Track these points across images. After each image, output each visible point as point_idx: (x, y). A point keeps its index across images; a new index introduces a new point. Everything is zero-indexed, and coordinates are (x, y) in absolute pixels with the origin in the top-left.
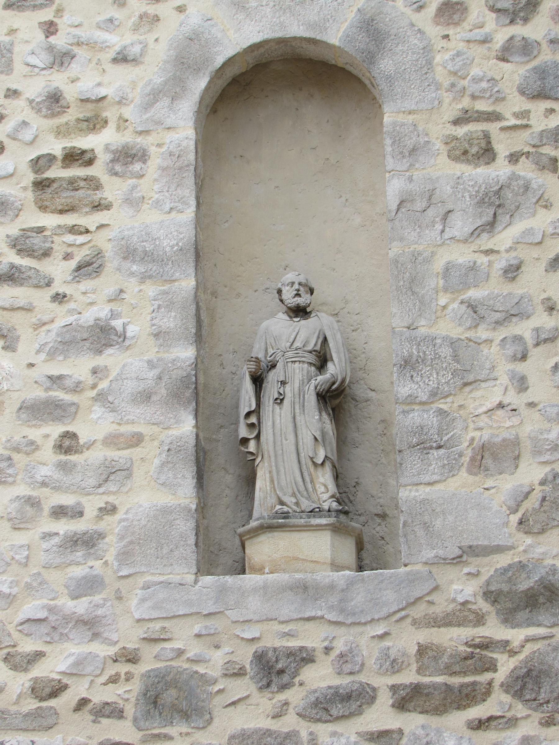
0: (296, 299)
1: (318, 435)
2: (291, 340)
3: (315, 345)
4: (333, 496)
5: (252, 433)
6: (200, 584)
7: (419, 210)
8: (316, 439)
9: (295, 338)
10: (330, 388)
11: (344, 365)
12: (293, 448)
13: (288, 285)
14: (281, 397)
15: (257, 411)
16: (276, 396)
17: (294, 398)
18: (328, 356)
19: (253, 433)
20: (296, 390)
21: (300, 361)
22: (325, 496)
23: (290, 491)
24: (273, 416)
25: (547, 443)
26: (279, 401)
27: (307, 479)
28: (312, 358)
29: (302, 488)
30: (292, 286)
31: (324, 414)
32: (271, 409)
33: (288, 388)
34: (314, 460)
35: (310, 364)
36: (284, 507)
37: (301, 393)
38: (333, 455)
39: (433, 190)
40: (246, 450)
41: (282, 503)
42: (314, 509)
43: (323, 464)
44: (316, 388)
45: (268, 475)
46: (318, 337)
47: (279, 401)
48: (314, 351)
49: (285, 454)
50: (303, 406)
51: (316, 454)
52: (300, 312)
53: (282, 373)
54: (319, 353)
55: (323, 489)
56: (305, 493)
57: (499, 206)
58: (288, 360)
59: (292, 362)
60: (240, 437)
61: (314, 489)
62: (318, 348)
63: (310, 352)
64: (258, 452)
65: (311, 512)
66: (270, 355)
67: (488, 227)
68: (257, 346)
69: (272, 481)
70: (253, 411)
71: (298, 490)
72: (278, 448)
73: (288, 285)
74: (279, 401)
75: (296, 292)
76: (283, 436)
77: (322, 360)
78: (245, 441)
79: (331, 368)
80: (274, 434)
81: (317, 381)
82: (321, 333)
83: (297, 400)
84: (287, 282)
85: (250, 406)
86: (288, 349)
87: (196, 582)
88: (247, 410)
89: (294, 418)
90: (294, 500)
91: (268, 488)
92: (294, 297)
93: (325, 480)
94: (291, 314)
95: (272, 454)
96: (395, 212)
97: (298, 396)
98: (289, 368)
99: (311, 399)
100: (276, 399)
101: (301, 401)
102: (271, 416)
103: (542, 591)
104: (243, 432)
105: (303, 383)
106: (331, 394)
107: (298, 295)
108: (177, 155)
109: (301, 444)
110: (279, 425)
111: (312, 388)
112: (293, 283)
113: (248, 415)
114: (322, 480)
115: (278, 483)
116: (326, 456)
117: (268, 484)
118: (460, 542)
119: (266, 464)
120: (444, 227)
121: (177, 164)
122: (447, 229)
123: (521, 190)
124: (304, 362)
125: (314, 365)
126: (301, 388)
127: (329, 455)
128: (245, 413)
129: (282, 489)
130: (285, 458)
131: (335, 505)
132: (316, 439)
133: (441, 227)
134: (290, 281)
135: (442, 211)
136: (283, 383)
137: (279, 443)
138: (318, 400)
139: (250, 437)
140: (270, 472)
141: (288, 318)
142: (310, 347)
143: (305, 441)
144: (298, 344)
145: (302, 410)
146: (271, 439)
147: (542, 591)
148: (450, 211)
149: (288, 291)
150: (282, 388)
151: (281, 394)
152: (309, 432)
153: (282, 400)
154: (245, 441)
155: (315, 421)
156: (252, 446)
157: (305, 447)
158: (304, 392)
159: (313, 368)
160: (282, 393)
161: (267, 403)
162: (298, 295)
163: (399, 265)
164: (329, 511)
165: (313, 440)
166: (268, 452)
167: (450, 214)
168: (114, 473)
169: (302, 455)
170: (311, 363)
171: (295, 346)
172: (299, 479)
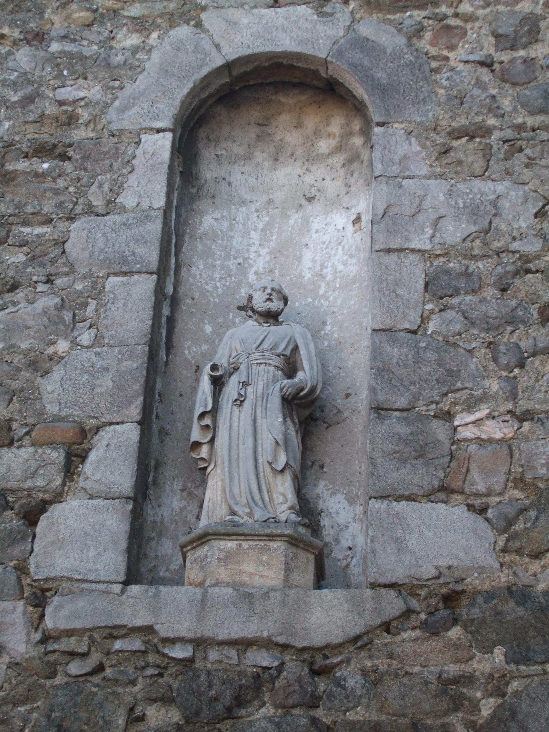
0: (267, 303)
1: (280, 438)
2: (259, 341)
3: (285, 349)
4: (292, 508)
5: (204, 438)
6: (128, 593)
7: (407, 214)
8: (277, 443)
9: (263, 341)
10: (298, 394)
11: (315, 373)
12: (250, 452)
13: (260, 290)
14: (242, 399)
15: (214, 412)
16: (236, 397)
17: (256, 401)
18: (299, 366)
19: (207, 437)
20: (260, 392)
21: (266, 364)
22: (284, 507)
23: (244, 501)
24: (231, 419)
25: (544, 457)
26: (240, 402)
27: (264, 488)
28: (278, 361)
29: (257, 497)
30: (264, 291)
31: (289, 422)
32: (229, 411)
33: (250, 389)
34: (273, 465)
35: (277, 367)
36: (236, 517)
37: (265, 396)
38: (295, 464)
39: (424, 196)
40: (198, 457)
41: (233, 513)
42: (268, 519)
43: (282, 471)
44: (281, 390)
45: (220, 484)
46: (289, 343)
47: (238, 403)
48: (283, 355)
49: (240, 460)
50: (266, 409)
51: (276, 459)
52: (271, 317)
53: (245, 373)
54: (289, 359)
55: (281, 499)
56: (260, 503)
57: (495, 215)
58: (252, 362)
59: (257, 364)
60: (192, 441)
61: (271, 499)
62: (288, 353)
63: (279, 356)
64: (211, 459)
65: (265, 521)
66: (233, 356)
67: (483, 234)
68: (220, 352)
69: (224, 491)
70: (209, 412)
71: (254, 501)
72: (234, 453)
73: (260, 290)
74: (238, 403)
75: (267, 297)
76: (241, 440)
77: (290, 367)
78: (197, 445)
79: (300, 375)
80: (230, 437)
81: (283, 385)
82: (292, 340)
83: (259, 403)
84: (259, 287)
85: (206, 406)
86: (254, 351)
87: (123, 592)
88: (201, 410)
89: (255, 421)
90: (247, 510)
91: (219, 498)
92: (266, 302)
93: (283, 490)
94: (261, 321)
95: (226, 458)
96: (381, 216)
97: (261, 399)
98: (254, 371)
99: (276, 402)
100: (236, 400)
101: (264, 404)
102: (228, 418)
103: (533, 621)
104: (196, 435)
105: (267, 386)
106: (299, 402)
107: (270, 300)
108: (151, 153)
109: (262, 474)
110: (237, 429)
111: (277, 389)
112: (265, 288)
113: (202, 415)
114: (281, 489)
115: (231, 491)
116: (287, 464)
117: (219, 493)
118: (438, 561)
119: (219, 471)
120: (434, 232)
121: (150, 162)
122: (438, 235)
123: (520, 201)
124: (270, 364)
125: (282, 370)
126: (265, 391)
127: (291, 463)
128: (199, 413)
129: (233, 497)
130: (241, 464)
131: (293, 517)
132: (277, 443)
133: (431, 232)
134: (262, 285)
135: (433, 216)
136: (246, 384)
137: (234, 447)
138: (283, 405)
139: (203, 441)
140: (222, 481)
141: (257, 324)
142: (280, 350)
143: (265, 446)
144: (265, 346)
145: (264, 414)
146: (226, 442)
147: (533, 621)
148: (441, 217)
149: (259, 296)
150: (244, 389)
151: (242, 396)
152: (270, 436)
153: (242, 402)
154: (197, 445)
155: (277, 423)
156: (204, 451)
157: (264, 453)
158: (268, 394)
159: (280, 373)
160: (243, 394)
161: (225, 406)
162: (270, 300)
163: (383, 267)
164: (286, 522)
165: (274, 444)
166: (223, 459)
167: (441, 220)
168: (43, 466)
169: (260, 461)
170: (278, 367)
171: (262, 347)
172: (255, 488)
